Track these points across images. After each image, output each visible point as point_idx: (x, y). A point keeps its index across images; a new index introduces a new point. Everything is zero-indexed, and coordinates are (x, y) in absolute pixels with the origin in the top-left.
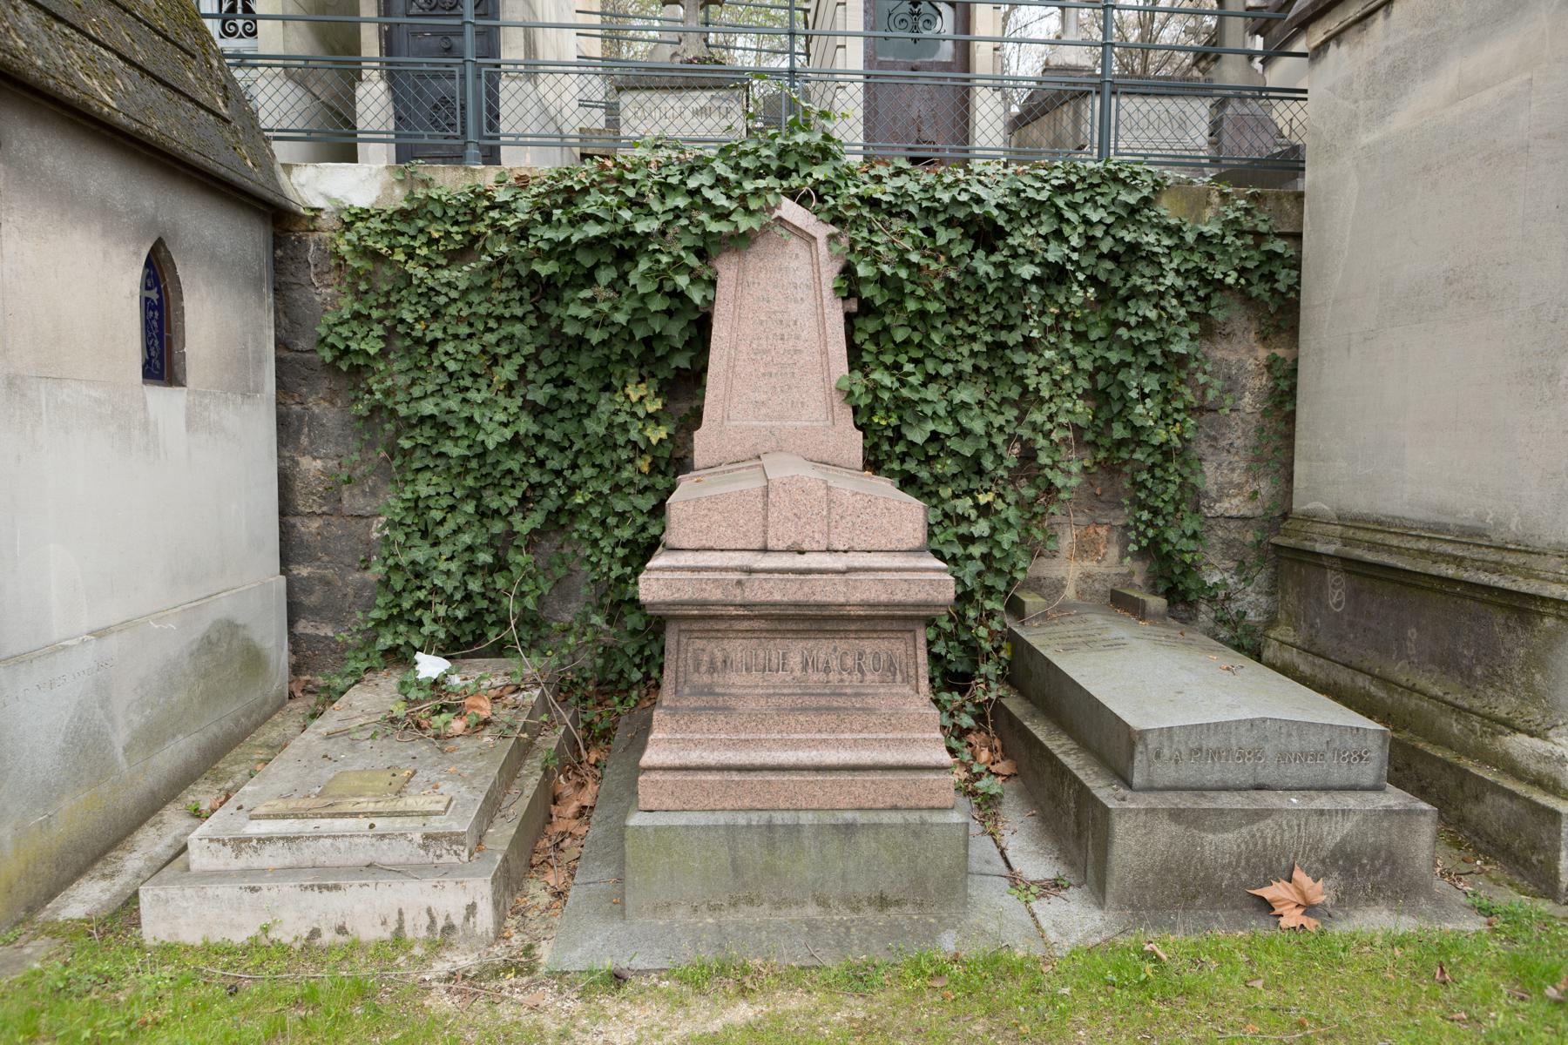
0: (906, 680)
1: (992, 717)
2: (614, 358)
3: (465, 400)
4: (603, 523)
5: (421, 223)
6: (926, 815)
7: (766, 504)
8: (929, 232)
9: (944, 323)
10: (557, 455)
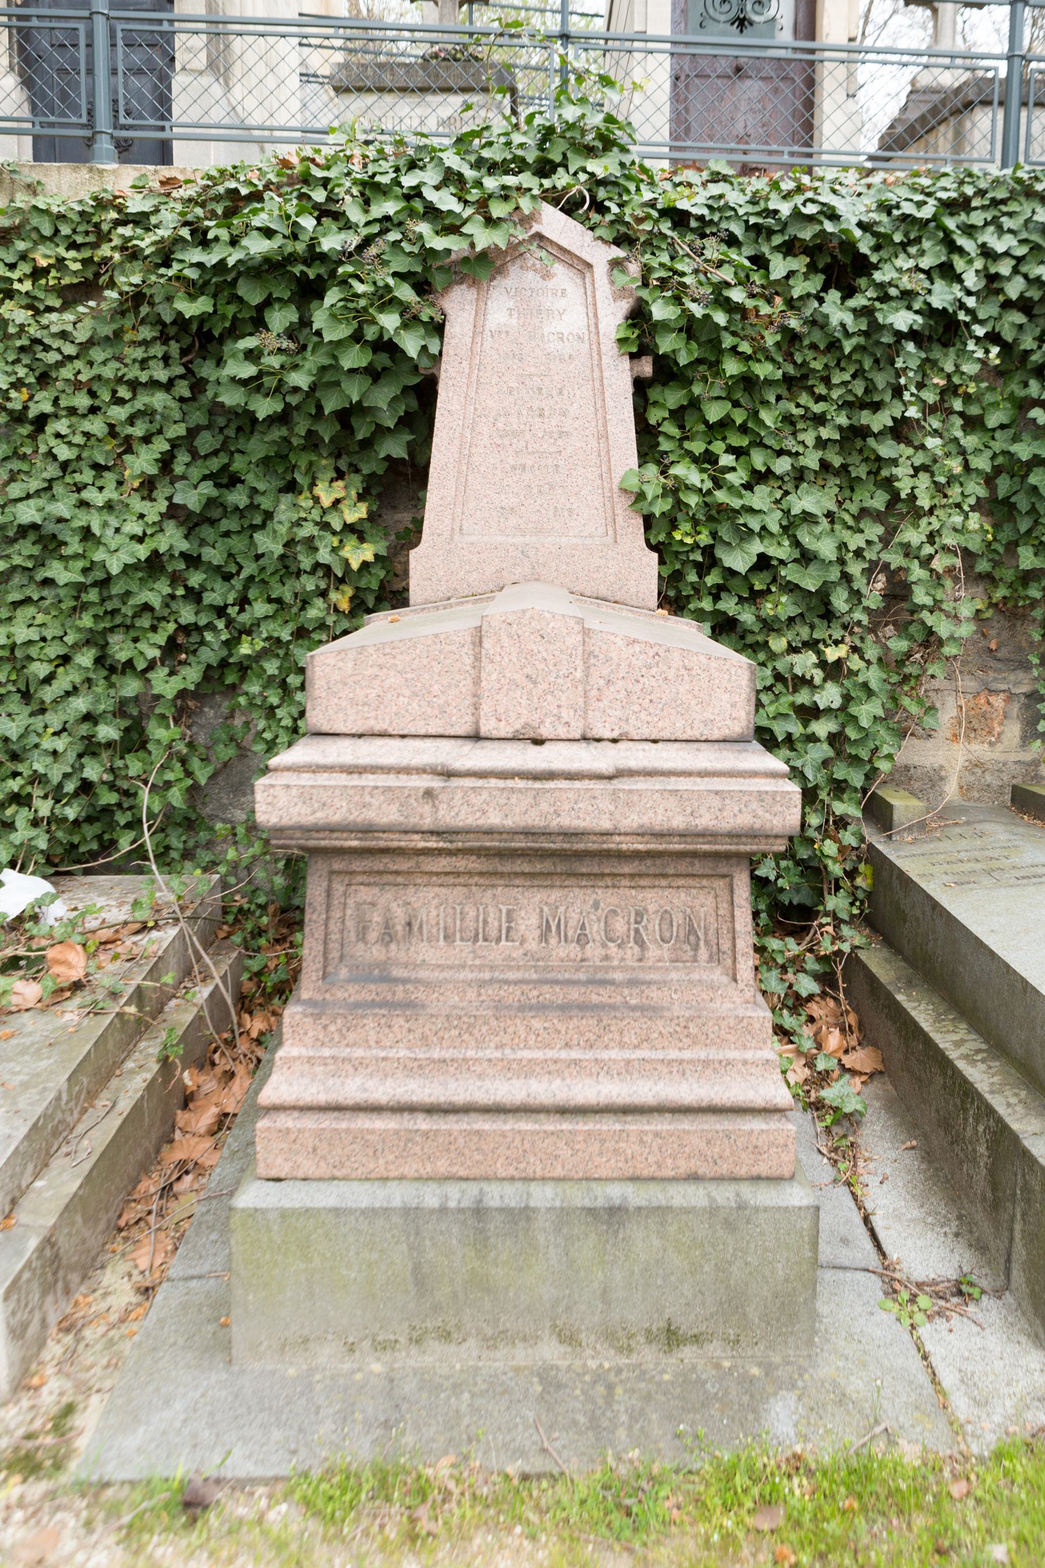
0: (716, 957)
1: (839, 975)
2: (295, 441)
3: (83, 504)
4: (284, 685)
5: (21, 246)
6: (746, 1190)
7: (478, 658)
8: (760, 262)
9: (779, 398)
10: (219, 585)
